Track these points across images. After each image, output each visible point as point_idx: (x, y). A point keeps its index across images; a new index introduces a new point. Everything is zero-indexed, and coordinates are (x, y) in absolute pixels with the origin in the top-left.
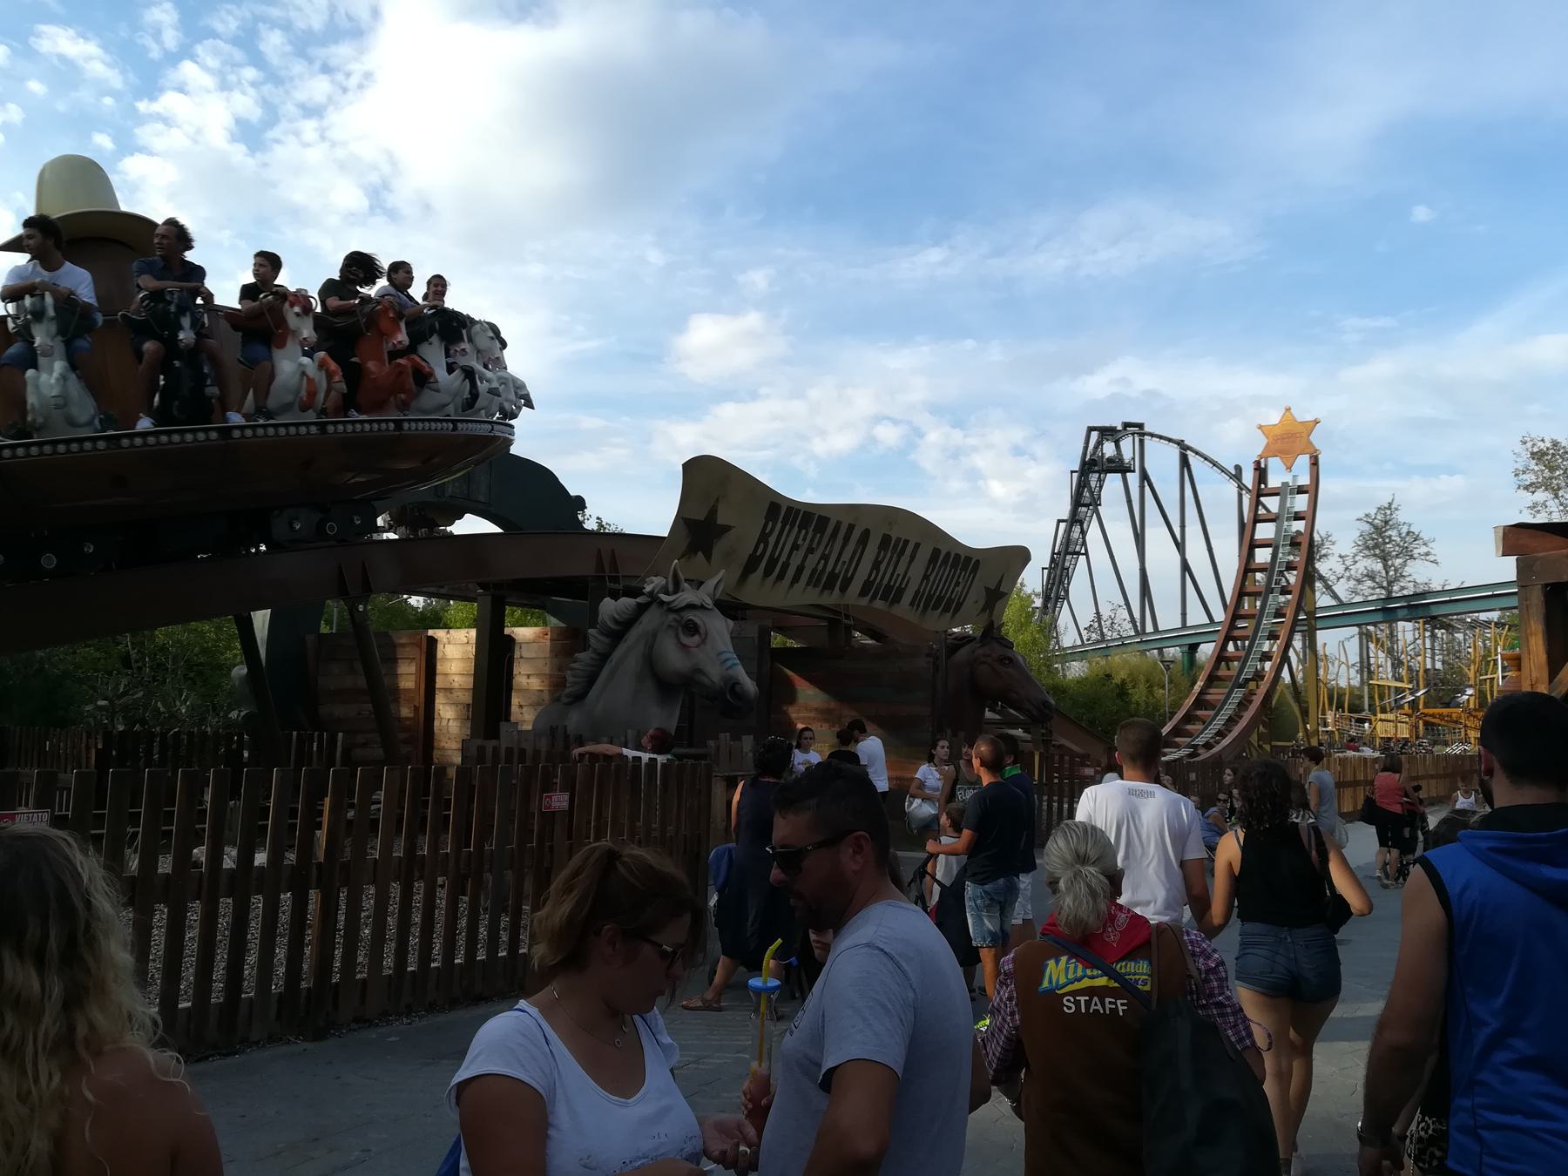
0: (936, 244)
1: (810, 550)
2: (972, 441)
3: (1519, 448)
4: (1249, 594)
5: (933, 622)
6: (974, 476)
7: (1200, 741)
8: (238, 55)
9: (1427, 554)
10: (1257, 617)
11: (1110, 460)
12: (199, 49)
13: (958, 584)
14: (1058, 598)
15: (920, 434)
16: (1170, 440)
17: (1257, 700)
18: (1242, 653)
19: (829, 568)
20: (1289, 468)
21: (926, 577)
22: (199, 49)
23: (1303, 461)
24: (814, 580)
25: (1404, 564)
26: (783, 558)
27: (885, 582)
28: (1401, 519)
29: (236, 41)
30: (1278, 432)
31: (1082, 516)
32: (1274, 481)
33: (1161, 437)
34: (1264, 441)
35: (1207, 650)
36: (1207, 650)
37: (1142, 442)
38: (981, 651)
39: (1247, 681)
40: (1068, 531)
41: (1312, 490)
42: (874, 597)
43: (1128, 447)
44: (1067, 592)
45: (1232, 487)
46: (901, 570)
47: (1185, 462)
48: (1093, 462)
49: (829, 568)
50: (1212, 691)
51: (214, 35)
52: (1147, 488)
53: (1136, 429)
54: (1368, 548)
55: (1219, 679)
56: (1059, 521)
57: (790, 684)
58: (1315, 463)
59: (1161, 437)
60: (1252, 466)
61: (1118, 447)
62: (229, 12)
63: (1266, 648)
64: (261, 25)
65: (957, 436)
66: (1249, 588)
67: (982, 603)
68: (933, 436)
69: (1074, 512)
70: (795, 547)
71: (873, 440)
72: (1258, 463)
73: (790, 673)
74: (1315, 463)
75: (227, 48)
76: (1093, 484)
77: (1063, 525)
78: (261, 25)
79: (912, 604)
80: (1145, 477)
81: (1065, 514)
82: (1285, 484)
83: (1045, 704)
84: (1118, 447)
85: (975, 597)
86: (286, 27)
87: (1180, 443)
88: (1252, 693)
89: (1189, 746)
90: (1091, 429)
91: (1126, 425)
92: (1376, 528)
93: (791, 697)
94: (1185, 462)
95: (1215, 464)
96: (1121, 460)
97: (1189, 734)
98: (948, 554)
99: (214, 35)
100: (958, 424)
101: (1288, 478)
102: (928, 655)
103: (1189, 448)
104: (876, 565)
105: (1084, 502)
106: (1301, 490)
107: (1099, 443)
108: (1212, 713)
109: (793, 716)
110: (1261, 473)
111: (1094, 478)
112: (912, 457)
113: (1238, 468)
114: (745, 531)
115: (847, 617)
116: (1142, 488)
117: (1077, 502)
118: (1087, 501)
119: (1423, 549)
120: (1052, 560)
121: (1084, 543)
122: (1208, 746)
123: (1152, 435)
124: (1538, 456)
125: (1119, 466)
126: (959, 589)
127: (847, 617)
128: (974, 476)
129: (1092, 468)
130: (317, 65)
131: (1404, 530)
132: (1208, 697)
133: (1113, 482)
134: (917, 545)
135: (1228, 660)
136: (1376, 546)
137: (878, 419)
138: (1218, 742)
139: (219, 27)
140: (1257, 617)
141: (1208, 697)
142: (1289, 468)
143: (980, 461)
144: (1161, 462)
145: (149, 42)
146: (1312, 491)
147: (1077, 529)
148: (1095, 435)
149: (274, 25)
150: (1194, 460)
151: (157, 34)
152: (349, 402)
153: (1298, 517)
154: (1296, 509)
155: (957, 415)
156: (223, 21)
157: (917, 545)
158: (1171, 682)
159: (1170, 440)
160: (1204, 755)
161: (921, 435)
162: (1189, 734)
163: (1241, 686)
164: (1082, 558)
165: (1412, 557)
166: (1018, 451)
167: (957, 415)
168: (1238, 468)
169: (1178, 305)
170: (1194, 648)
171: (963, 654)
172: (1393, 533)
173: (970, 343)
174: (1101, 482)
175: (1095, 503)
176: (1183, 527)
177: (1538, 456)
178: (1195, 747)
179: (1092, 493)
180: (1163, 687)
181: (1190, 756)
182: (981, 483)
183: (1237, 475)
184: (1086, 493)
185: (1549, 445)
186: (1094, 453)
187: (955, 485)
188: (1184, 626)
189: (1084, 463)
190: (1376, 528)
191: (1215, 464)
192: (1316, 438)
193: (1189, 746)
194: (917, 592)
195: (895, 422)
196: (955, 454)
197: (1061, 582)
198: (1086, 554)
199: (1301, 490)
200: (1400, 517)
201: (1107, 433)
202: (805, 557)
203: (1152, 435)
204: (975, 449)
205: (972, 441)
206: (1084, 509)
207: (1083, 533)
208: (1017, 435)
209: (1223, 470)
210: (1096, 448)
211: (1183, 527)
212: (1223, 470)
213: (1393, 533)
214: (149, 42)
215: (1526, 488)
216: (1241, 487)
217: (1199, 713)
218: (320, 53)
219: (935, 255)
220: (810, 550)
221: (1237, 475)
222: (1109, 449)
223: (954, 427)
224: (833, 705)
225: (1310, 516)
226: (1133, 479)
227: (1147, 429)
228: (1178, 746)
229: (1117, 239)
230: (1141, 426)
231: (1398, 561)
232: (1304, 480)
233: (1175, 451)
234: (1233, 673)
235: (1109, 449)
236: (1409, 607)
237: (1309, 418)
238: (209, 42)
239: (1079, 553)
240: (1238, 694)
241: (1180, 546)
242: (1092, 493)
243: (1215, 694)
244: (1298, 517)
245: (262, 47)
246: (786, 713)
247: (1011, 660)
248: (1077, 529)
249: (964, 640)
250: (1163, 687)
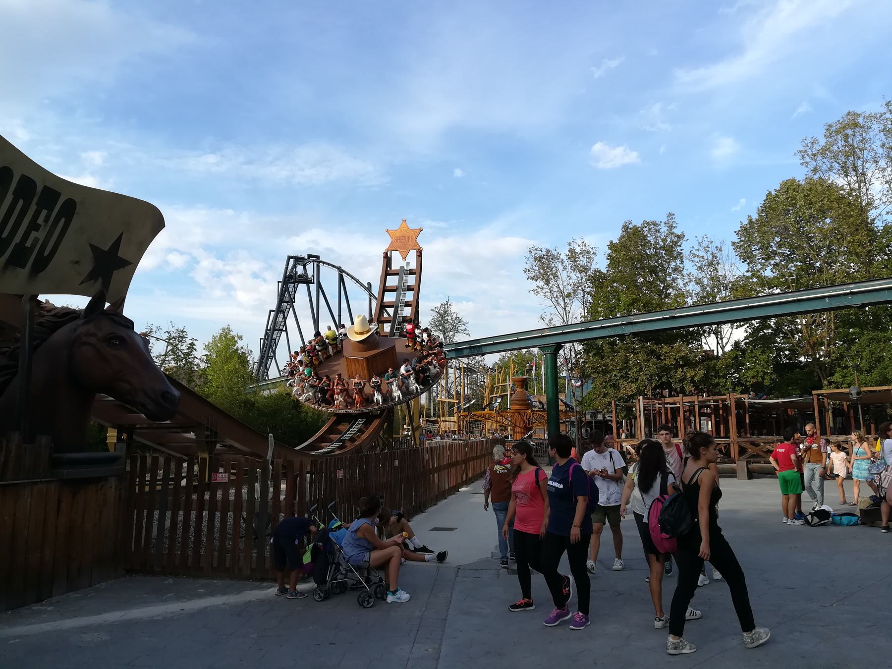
0: (213, 152)
2: (228, 268)
3: (528, 255)
7: (347, 436)
9: (465, 330)
11: (300, 276)
13: (34, 226)
16: (334, 266)
20: (404, 258)
23: (413, 254)
25: (454, 335)
28: (453, 311)
30: (398, 235)
31: (284, 308)
32: (395, 266)
33: (329, 264)
37: (318, 266)
38: (82, 330)
40: (276, 317)
41: (417, 272)
44: (274, 353)
48: (290, 277)
54: (436, 326)
56: (271, 311)
58: (420, 256)
59: (329, 264)
61: (305, 269)
65: (220, 264)
68: (205, 263)
71: (167, 263)
72: (386, 254)
74: (420, 256)
76: (290, 290)
77: (273, 313)
80: (319, 286)
82: (402, 268)
84: (305, 269)
87: (339, 268)
89: (339, 440)
90: (290, 257)
91: (310, 256)
95: (357, 281)
96: (307, 276)
97: (339, 432)
100: (221, 257)
101: (404, 264)
103: (344, 271)
105: (285, 299)
106: (411, 272)
107: (294, 266)
110: (388, 260)
111: (291, 286)
113: (369, 284)
117: (281, 300)
118: (287, 299)
119: (463, 327)
120: (266, 334)
121: (285, 324)
122: (352, 440)
124: (539, 259)
126: (41, 234)
129: (290, 280)
131: (454, 316)
133: (302, 287)
136: (440, 325)
137: (171, 250)
138: (359, 437)
142: (404, 258)
143: (233, 280)
144: (329, 279)
147: (281, 316)
148: (292, 261)
150: (346, 279)
155: (220, 252)
159: (334, 266)
160: (350, 446)
161: (198, 262)
162: (339, 432)
164: (284, 333)
165: (458, 331)
166: (255, 276)
167: (220, 252)
168: (369, 284)
169: (343, 204)
171: (62, 334)
172: (449, 318)
173: (230, 212)
174: (295, 289)
175: (292, 301)
176: (340, 316)
177: (539, 259)
178: (343, 441)
179: (290, 295)
181: (340, 448)
182: (232, 293)
183: (369, 288)
185: (544, 253)
186: (292, 271)
187: (218, 293)
189: (285, 277)
191: (357, 281)
193: (339, 440)
195: (181, 253)
196: (218, 275)
197: (271, 347)
198: (286, 331)
199: (411, 272)
200: (453, 309)
201: (299, 260)
203: (324, 263)
204: (230, 273)
205: (228, 268)
207: (285, 318)
208: (256, 266)
209: (362, 285)
210: (292, 268)
211: (340, 316)
212: (362, 285)
213: (449, 318)
215: (532, 279)
216: (371, 295)
219: (211, 159)
221: (369, 288)
223: (218, 259)
225: (416, 289)
226: (313, 287)
227: (321, 259)
228: (331, 441)
229: (311, 165)
230: (318, 257)
231: (451, 333)
232: (413, 266)
233: (336, 273)
235: (300, 270)
236: (471, 348)
239: (282, 330)
242: (290, 295)
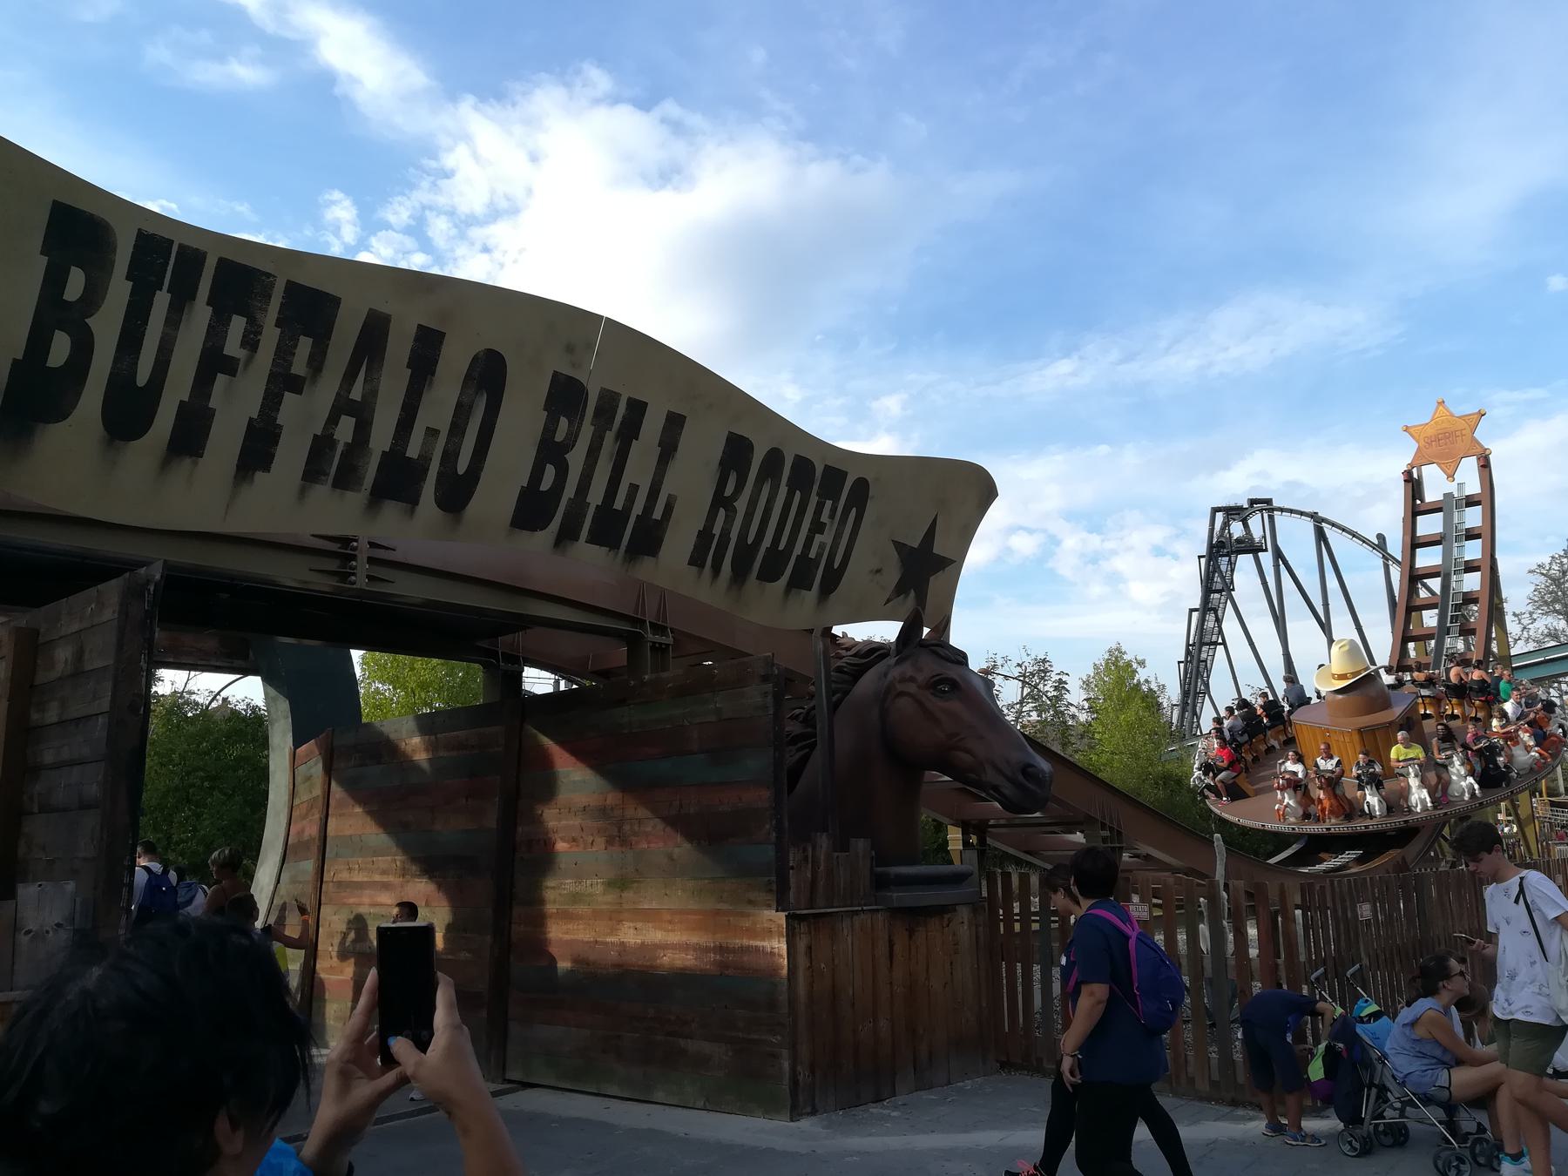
1: (283, 382)
2: (1109, 545)
4: (1414, 639)
5: (769, 611)
6: (1115, 579)
8: (410, 243)
11: (1238, 541)
12: (373, 241)
13: (818, 527)
14: (1196, 694)
15: (1055, 541)
16: (1302, 513)
20: (1451, 476)
21: (720, 501)
22: (373, 241)
26: (177, 389)
27: (595, 497)
29: (408, 231)
30: (1430, 432)
32: (1431, 495)
33: (1291, 511)
34: (1414, 446)
37: (1271, 518)
38: (895, 673)
40: (1202, 620)
41: (1486, 499)
42: (567, 534)
44: (1207, 685)
46: (639, 469)
48: (1221, 545)
51: (388, 226)
52: (1282, 567)
53: (1264, 505)
54: (1546, 603)
56: (1192, 611)
57: (546, 762)
58: (1485, 465)
59: (1291, 511)
61: (1246, 526)
62: (400, 204)
65: (1095, 541)
67: (893, 575)
69: (1206, 599)
70: (214, 363)
71: (1009, 551)
75: (399, 237)
76: (1223, 568)
77: (1195, 615)
79: (697, 560)
80: (1278, 555)
81: (1197, 604)
82: (1448, 496)
83: (1027, 770)
84: (1246, 526)
85: (872, 556)
86: (451, 213)
87: (1313, 516)
90: (1215, 510)
91: (1252, 502)
92: (1553, 580)
93: (547, 788)
94: (1321, 536)
95: (1354, 535)
96: (1252, 539)
98: (775, 457)
99: (388, 226)
100: (1095, 528)
101: (1452, 488)
102: (765, 679)
103: (1324, 520)
104: (551, 451)
105: (1215, 586)
106: (1471, 502)
107: (1226, 525)
109: (551, 824)
111: (1224, 561)
112: (1050, 565)
114: (930, 667)
115: (658, 629)
116: (1277, 567)
117: (1208, 589)
118: (1219, 587)
120: (1188, 652)
121: (1221, 632)
123: (1282, 510)
125: (1250, 547)
126: (826, 538)
127: (658, 629)
128: (1115, 579)
129: (1221, 552)
130: (478, 246)
133: (1245, 562)
139: (392, 219)
142: (1451, 476)
143: (1120, 564)
144: (1296, 538)
145: (331, 238)
146: (1486, 501)
147: (1211, 617)
149: (440, 212)
150: (1330, 532)
151: (337, 231)
152: (1306, 816)
153: (1471, 535)
155: (1093, 520)
156: (396, 213)
157: (675, 423)
159: (1302, 513)
164: (1220, 649)
167: (1093, 520)
168: (1381, 537)
171: (868, 681)
174: (1232, 565)
175: (1228, 588)
179: (1223, 578)
183: (1380, 545)
184: (1217, 578)
187: (1096, 590)
189: (1211, 546)
190: (1553, 580)
191: (1354, 535)
192: (1484, 435)
195: (1030, 531)
196: (1094, 559)
198: (1224, 643)
199: (1471, 502)
201: (1232, 512)
202: (272, 401)
203: (1282, 510)
204: (1114, 553)
206: (1217, 596)
207: (1219, 621)
209: (1364, 541)
210: (1223, 529)
212: (1364, 541)
216: (1387, 557)
218: (476, 233)
220: (283, 382)
222: (1237, 529)
223: (1090, 532)
224: (613, 798)
226: (1266, 558)
227: (1276, 504)
229: (1241, 337)
230: (1269, 502)
232: (1474, 487)
233: (1309, 525)
235: (1237, 529)
237: (1469, 409)
238: (382, 234)
239: (1216, 644)
241: (1326, 627)
242: (1223, 578)
244: (1471, 535)
245: (430, 234)
246: (538, 821)
247: (954, 685)
248: (1211, 617)
249: (874, 652)
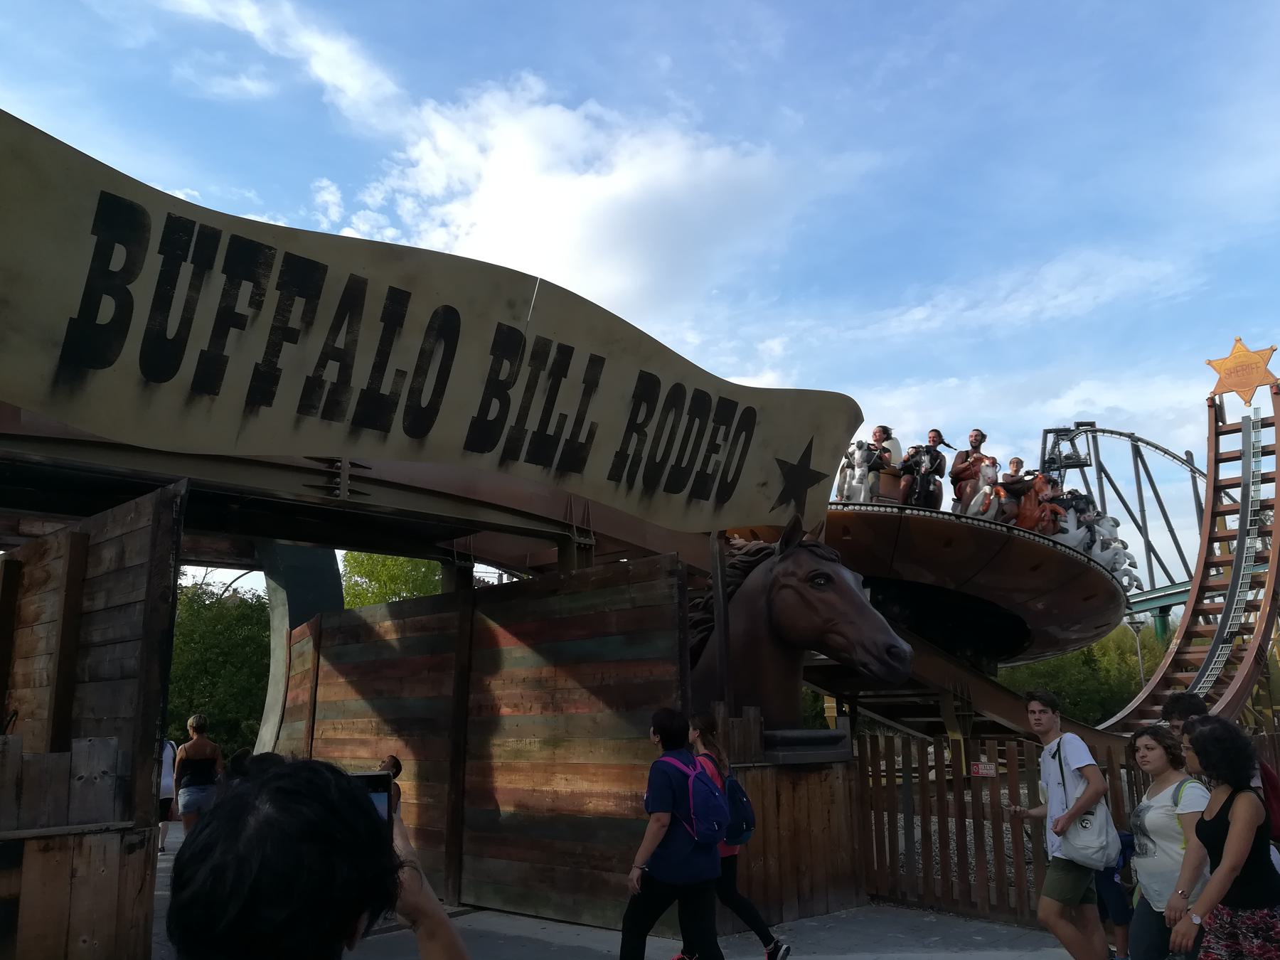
1: (282, 334)
8: (383, 220)
10: (1234, 564)
11: (1067, 457)
12: (354, 219)
13: (713, 448)
16: (1121, 434)
17: (1249, 656)
18: (1233, 557)
19: (360, 379)
21: (634, 427)
22: (354, 219)
24: (318, 400)
26: (199, 341)
27: (532, 424)
29: (381, 210)
30: (1229, 365)
32: (1232, 418)
33: (1112, 432)
35: (1178, 614)
36: (1178, 614)
37: (1095, 438)
38: (779, 569)
39: (1233, 635)
42: (510, 455)
43: (1082, 443)
45: (1186, 473)
46: (567, 402)
47: (1137, 453)
48: (1052, 461)
49: (360, 379)
50: (1191, 649)
51: (365, 207)
52: (1105, 479)
53: (1089, 427)
55: (1199, 635)
57: (492, 642)
59: (1112, 432)
60: (1206, 404)
61: (1073, 445)
62: (376, 188)
63: (1250, 596)
64: (397, 195)
66: (1212, 582)
67: (776, 487)
70: (227, 320)
73: (494, 625)
78: (397, 195)
79: (614, 476)
80: (1101, 469)
82: (1246, 419)
84: (1073, 445)
87: (1130, 436)
88: (1241, 649)
90: (1047, 432)
91: (1079, 425)
93: (494, 663)
94: (1137, 453)
96: (1078, 456)
98: (678, 390)
99: (365, 207)
101: (1249, 412)
102: (671, 573)
103: (1140, 440)
104: (496, 388)
107: (1056, 444)
108: (1196, 674)
109: (498, 693)
113: (1189, 454)
115: (583, 532)
116: (1100, 479)
123: (1104, 431)
126: (721, 457)
132: (1188, 657)
134: (596, 363)
135: (1205, 613)
139: (369, 200)
140: (1234, 564)
141: (1188, 657)
142: (1248, 402)
144: (1116, 456)
145: (321, 217)
151: (325, 210)
154: (1263, 444)
156: (372, 196)
157: (596, 363)
158: (1144, 647)
159: (1121, 434)
163: (1225, 641)
168: (1189, 454)
170: (1165, 611)
176: (1142, 511)
180: (1136, 654)
183: (1189, 460)
188: (1153, 589)
189: (1044, 462)
191: (1166, 452)
194: (621, 456)
201: (1061, 433)
202: (273, 350)
203: (1104, 431)
209: (1175, 457)
210: (1053, 448)
211: (1142, 511)
212: (1175, 457)
214: (321, 217)
216: (1194, 471)
217: (1179, 675)
218: (436, 211)
220: (282, 334)
222: (1065, 448)
224: (547, 671)
226: (1091, 472)
227: (1098, 426)
230: (1092, 424)
233: (1127, 444)
234: (1215, 627)
235: (1065, 448)
237: (1264, 345)
240: (1224, 652)
243: (1197, 651)
245: (399, 212)
246: (487, 690)
250: (1136, 654)
